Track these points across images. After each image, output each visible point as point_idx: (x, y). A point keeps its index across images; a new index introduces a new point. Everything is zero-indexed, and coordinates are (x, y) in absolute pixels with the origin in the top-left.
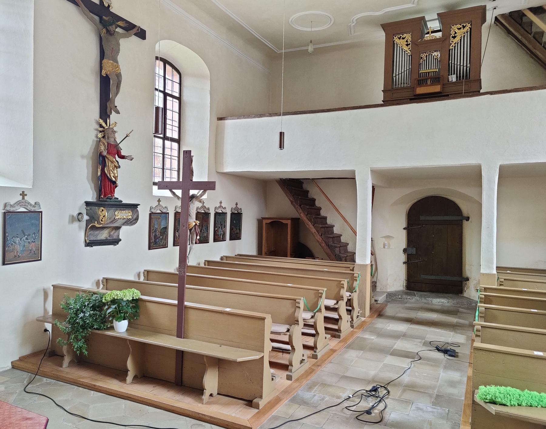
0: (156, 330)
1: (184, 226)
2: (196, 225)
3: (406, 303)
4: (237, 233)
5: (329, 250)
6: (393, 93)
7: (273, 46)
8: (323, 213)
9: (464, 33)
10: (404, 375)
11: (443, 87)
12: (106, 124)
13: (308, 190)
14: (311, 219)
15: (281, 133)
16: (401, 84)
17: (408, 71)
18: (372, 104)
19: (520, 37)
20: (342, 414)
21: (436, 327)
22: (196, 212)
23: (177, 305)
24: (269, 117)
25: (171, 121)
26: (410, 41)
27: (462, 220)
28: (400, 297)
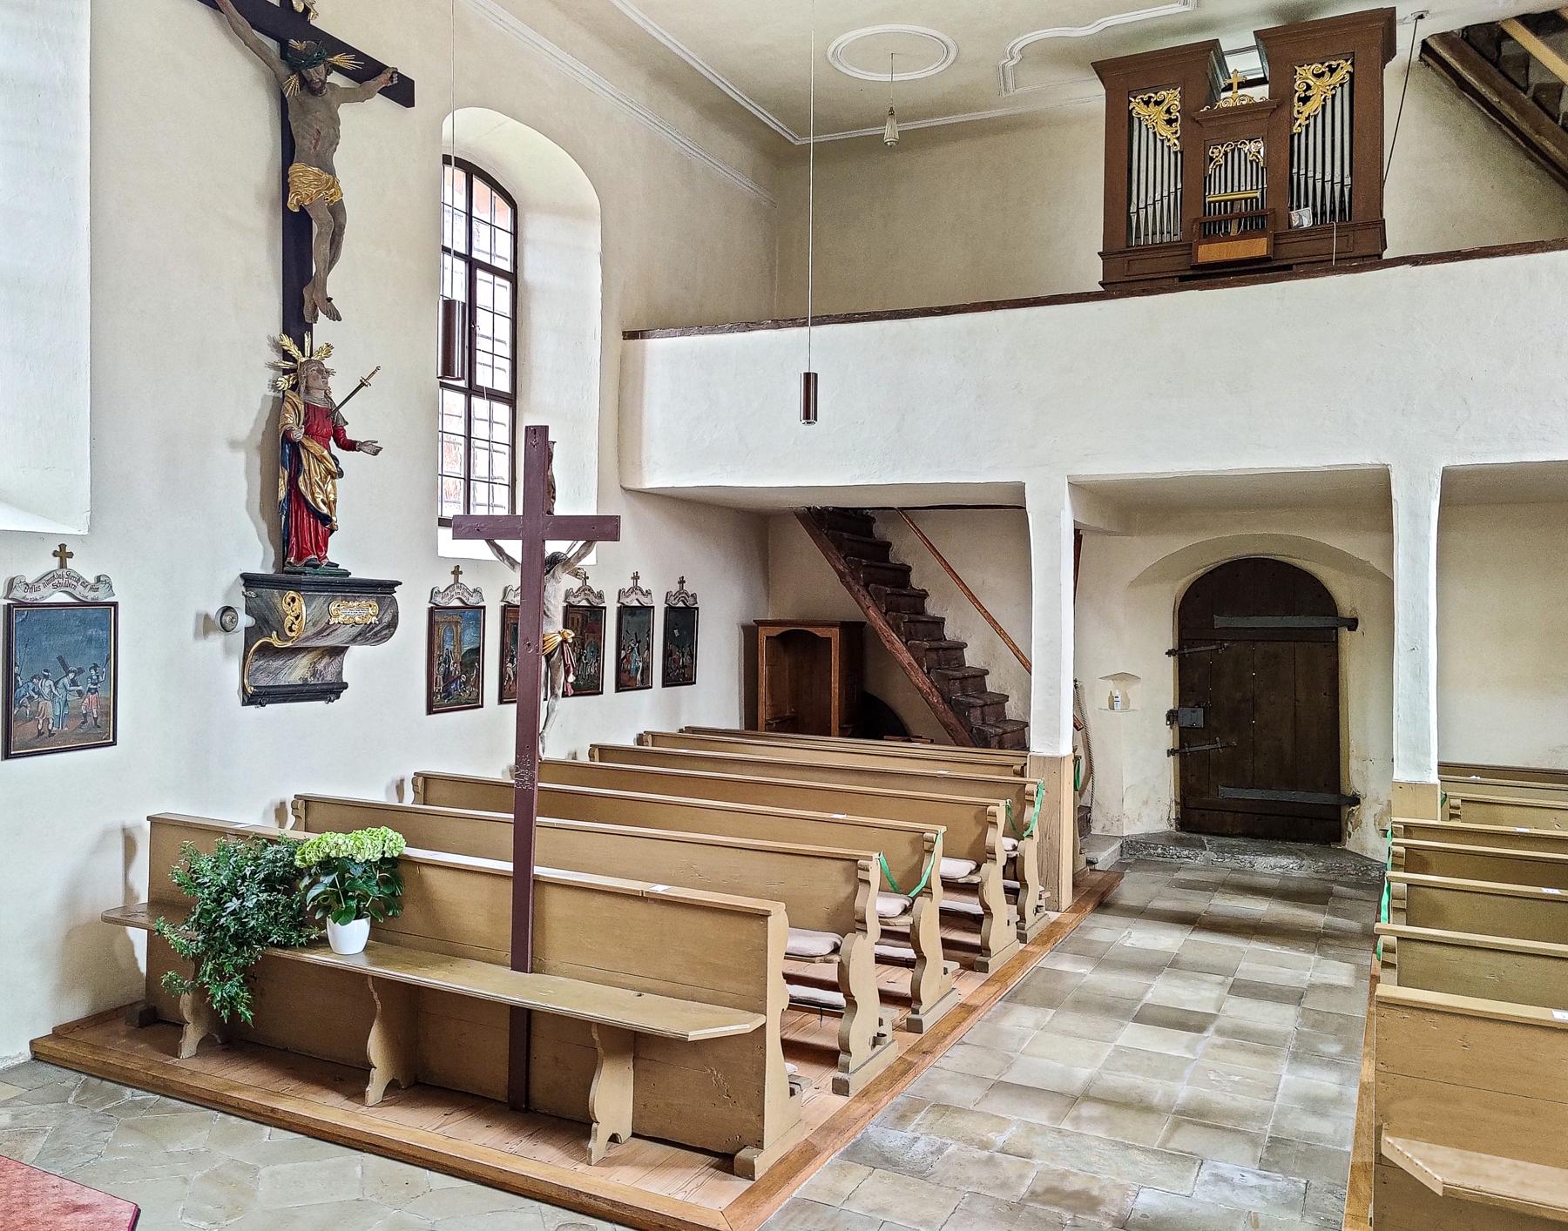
0: (451, 950)
1: (529, 645)
2: (565, 641)
3: (1179, 869)
5: (951, 714)
8: (932, 608)
9: (1334, 88)
12: (302, 349)
14: (898, 627)
15: (807, 376)
16: (1154, 233)
17: (1172, 197)
21: (1266, 941)
22: (565, 604)
26: (1179, 111)
27: (1337, 629)
28: (1159, 851)
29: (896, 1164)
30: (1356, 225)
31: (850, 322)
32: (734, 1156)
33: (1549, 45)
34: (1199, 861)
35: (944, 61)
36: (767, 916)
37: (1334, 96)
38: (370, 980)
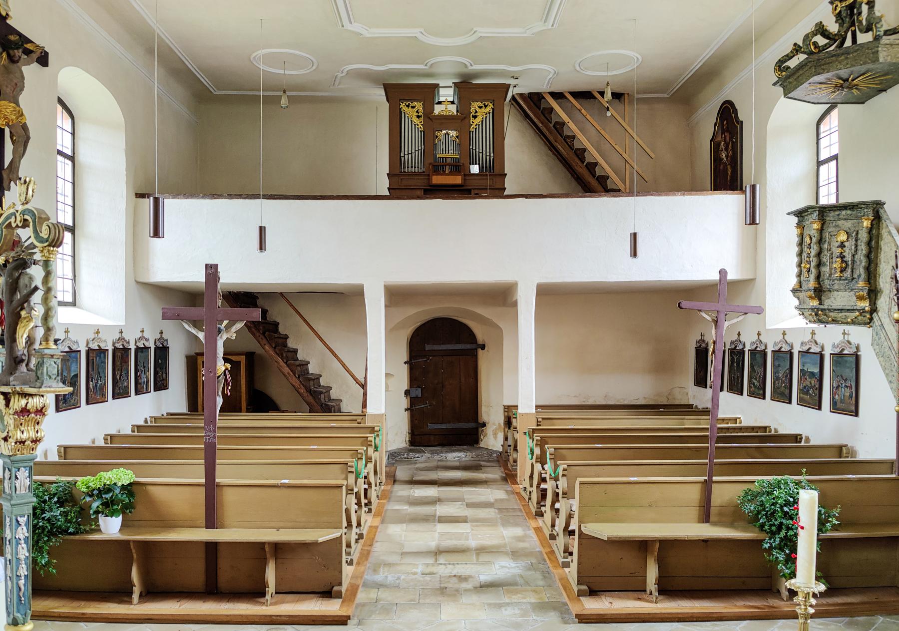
0: (169, 524)
1: (210, 372)
2: (227, 369)
5: (311, 397)
6: (401, 179)
7: (209, 83)
8: (291, 344)
9: (486, 114)
11: (464, 179)
14: (282, 354)
15: (261, 228)
16: (412, 167)
17: (420, 151)
18: (384, 195)
19: (540, 125)
21: (468, 487)
22: (87, 349)
23: (204, 484)
24: (229, 199)
25: (63, 196)
27: (477, 349)
28: (406, 456)
29: (386, 586)
30: (496, 175)
31: (273, 199)
32: (331, 592)
34: (423, 459)
35: (311, 68)
36: (342, 487)
37: (486, 117)
38: (132, 544)
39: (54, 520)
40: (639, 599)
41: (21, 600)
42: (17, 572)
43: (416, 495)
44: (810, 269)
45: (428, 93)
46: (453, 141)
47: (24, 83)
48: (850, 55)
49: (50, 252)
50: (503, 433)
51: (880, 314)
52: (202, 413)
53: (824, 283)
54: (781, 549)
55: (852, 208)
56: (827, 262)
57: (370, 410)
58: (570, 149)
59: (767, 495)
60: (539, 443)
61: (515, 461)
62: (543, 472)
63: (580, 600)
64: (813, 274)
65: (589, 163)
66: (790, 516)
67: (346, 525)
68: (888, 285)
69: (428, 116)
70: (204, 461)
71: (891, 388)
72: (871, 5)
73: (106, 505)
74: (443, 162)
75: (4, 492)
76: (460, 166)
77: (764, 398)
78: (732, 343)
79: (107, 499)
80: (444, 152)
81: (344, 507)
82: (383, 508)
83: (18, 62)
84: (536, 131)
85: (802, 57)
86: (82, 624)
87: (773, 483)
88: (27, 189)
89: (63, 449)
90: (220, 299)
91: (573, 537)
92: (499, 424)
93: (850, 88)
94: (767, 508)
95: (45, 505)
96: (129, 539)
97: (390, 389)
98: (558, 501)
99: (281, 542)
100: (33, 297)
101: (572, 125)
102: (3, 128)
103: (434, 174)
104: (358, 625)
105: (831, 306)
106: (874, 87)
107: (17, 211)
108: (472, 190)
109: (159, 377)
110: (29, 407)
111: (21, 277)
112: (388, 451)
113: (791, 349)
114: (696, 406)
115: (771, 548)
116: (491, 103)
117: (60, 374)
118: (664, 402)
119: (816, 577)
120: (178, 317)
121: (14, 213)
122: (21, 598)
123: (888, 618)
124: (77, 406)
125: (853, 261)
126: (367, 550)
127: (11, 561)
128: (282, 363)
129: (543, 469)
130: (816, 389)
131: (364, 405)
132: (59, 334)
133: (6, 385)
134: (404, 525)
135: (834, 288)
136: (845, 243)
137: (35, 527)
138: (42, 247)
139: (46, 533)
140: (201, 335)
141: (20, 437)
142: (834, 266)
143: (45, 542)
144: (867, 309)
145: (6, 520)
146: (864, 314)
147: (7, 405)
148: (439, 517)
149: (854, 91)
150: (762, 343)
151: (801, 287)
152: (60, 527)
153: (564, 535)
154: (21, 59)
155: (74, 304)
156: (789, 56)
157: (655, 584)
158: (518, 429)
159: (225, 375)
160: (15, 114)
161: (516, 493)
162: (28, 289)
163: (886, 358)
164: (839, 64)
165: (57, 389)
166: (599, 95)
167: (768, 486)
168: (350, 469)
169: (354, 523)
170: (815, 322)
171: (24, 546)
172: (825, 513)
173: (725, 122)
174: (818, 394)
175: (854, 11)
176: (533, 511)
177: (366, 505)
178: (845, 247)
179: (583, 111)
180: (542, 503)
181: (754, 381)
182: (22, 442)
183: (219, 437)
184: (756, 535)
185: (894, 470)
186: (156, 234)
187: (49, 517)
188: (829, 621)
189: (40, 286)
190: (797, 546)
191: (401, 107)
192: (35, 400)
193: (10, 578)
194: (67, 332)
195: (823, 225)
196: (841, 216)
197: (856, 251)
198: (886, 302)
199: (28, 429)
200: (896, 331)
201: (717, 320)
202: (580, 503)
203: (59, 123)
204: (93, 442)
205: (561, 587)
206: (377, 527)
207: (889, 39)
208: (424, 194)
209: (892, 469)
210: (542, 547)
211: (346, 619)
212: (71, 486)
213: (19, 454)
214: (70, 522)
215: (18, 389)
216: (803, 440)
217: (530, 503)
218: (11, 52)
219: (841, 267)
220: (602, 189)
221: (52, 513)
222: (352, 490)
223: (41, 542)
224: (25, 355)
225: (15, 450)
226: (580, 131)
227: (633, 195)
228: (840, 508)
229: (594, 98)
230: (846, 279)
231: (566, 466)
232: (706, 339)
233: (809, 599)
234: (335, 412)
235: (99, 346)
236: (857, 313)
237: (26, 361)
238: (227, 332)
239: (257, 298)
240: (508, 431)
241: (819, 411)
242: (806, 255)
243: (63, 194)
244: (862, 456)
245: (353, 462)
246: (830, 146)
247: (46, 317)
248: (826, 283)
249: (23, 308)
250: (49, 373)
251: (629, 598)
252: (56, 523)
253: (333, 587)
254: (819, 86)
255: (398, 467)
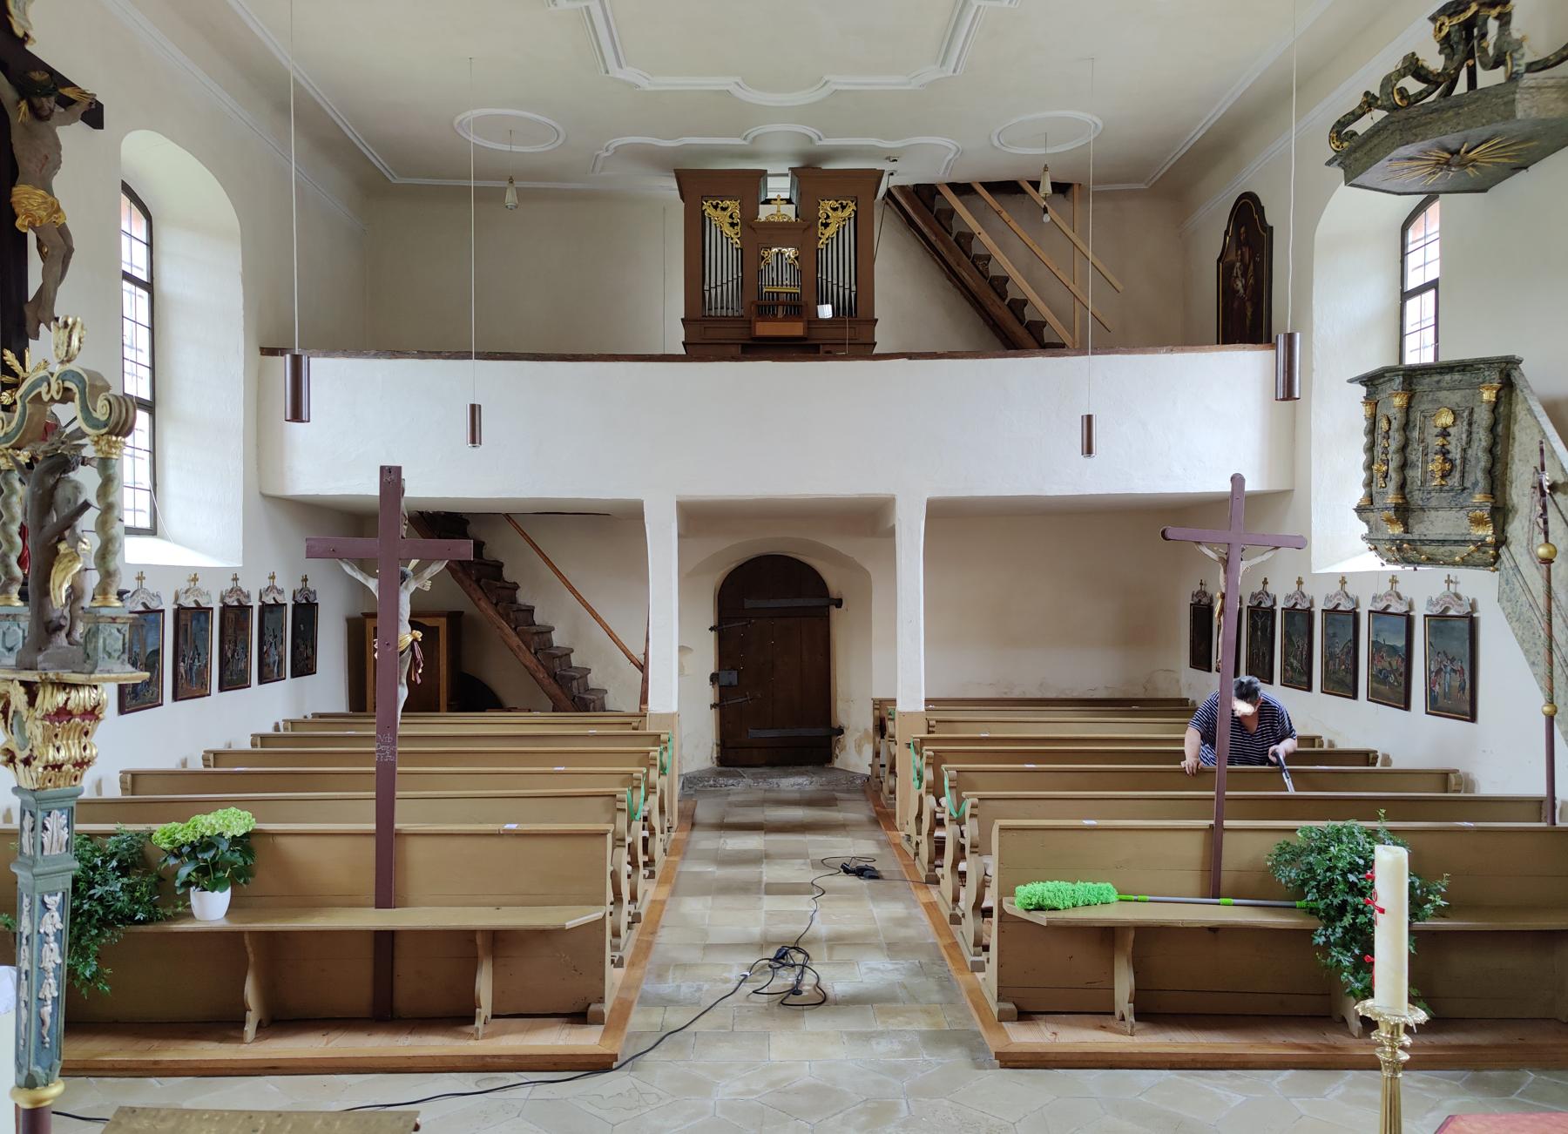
2: (415, 640)
3: (729, 794)
4: (308, 658)
8: (523, 597)
9: (844, 220)
10: (813, 923)
11: (808, 329)
12: (23, 364)
13: (483, 540)
14: (508, 615)
15: (473, 407)
16: (722, 308)
18: (677, 353)
19: (933, 238)
20: (747, 1004)
21: (815, 834)
22: (222, 605)
24: (419, 358)
27: (828, 607)
28: (712, 782)
30: (860, 321)
33: (960, 200)
34: (741, 787)
37: (844, 226)
38: (246, 937)
39: (110, 899)
40: (1103, 1028)
41: (43, 1043)
42: (38, 992)
43: (728, 848)
44: (1387, 473)
45: (749, 185)
46: (790, 264)
47: (60, 156)
48: (1463, 108)
49: (112, 444)
50: (872, 745)
51: (1512, 548)
52: (373, 714)
53: (1412, 496)
54: (1346, 946)
55: (1463, 370)
56: (1418, 461)
57: (654, 706)
58: (982, 278)
59: (1319, 854)
60: (931, 761)
61: (893, 792)
62: (938, 809)
63: (1003, 1028)
64: (1393, 482)
65: (1013, 301)
66: (1359, 890)
67: (613, 899)
68: (1526, 500)
69: (749, 223)
70: (375, 793)
71: (1535, 675)
72: (1503, 21)
73: (203, 871)
74: (773, 299)
75: (21, 853)
76: (801, 306)
77: (1309, 689)
78: (1253, 596)
79: (205, 861)
80: (775, 283)
81: (609, 869)
82: (674, 869)
83: (47, 118)
84: (925, 248)
85: (1378, 115)
86: (153, 1080)
87: (1329, 833)
88: (70, 337)
89: (129, 776)
90: (405, 524)
91: (989, 919)
92: (866, 730)
93: (1463, 165)
94: (1319, 875)
95: (94, 874)
96: (242, 929)
97: (686, 673)
98: (964, 858)
99: (501, 928)
100: (80, 519)
101: (985, 238)
102: (24, 231)
103: (759, 319)
104: (630, 1071)
105: (1425, 535)
106: (1504, 163)
107: (52, 374)
108: (821, 347)
109: (301, 654)
110: (71, 705)
111: (60, 485)
112: (683, 775)
113: (1355, 606)
114: (1194, 702)
115: (1328, 943)
116: (852, 202)
117: (127, 650)
118: (1139, 694)
119: (1409, 997)
120: (334, 554)
121: (47, 377)
122: (44, 1038)
123: (1544, 1075)
124: (156, 703)
125: (1464, 460)
126: (647, 941)
127: (29, 973)
128: (508, 630)
129: (939, 804)
130: (1401, 675)
131: (644, 699)
132: (126, 582)
133: (30, 669)
134: (709, 899)
135: (1430, 505)
136: (1450, 430)
137: (75, 912)
138: (97, 436)
139: (94, 921)
140: (373, 584)
141: (54, 757)
142: (1431, 467)
143: (92, 938)
144: (1489, 539)
145: (22, 902)
146: (1484, 549)
147: (32, 702)
148: (767, 885)
149: (1470, 171)
150: (1304, 597)
151: (1372, 504)
152: (120, 911)
153: (974, 915)
154: (54, 113)
155: (152, 531)
156: (1356, 114)
157: (1129, 1003)
158: (897, 738)
159: (412, 649)
160: (45, 209)
161: (895, 845)
162: (72, 507)
163: (1525, 624)
164: (1443, 126)
165: (123, 676)
166: (1030, 186)
167: (1320, 838)
168: (619, 805)
169: (626, 896)
170: (1396, 562)
171: (54, 946)
172: (1421, 887)
173: (1243, 229)
174: (1403, 683)
175: (1473, 32)
176: (923, 875)
177: (645, 864)
178: (1449, 435)
179: (1004, 214)
180: (937, 862)
181: (1292, 660)
182: (57, 766)
183: (400, 753)
184: (1300, 921)
185: (1543, 816)
186: (297, 415)
187: (102, 895)
188: (1436, 1076)
189: (93, 500)
190: (1373, 942)
191: (704, 208)
192: (81, 694)
193: (26, 1003)
194: (140, 578)
195: (1410, 400)
196: (1443, 384)
197: (1469, 442)
198: (1523, 528)
199: (68, 744)
200: (1543, 577)
201: (1228, 558)
202: (1001, 862)
203: (125, 226)
204: (184, 764)
205: (970, 1005)
206: (663, 903)
207: (1535, 79)
208: (742, 353)
209: (1541, 813)
210: (937, 936)
211: (609, 1061)
212: (142, 840)
213: (51, 787)
214: (138, 901)
215: (51, 675)
216: (1379, 760)
217: (917, 861)
218: (36, 101)
219: (1443, 470)
220: (1036, 344)
221: (107, 888)
222: (624, 840)
223: (85, 938)
224: (65, 617)
225: (44, 780)
226: (999, 248)
227: (1086, 354)
228: (1448, 878)
229: (1022, 191)
230: (1452, 490)
231: (976, 800)
232: (1209, 590)
233: (1398, 1035)
234: (595, 711)
235: (196, 602)
236: (1472, 547)
237: (67, 628)
238: (416, 579)
239: (467, 522)
240: (880, 742)
241: (1355, 701)
242: (1380, 450)
243: (135, 346)
244: (1485, 789)
245: (624, 793)
246: (1424, 264)
247: (105, 553)
248: (1416, 497)
249: (61, 539)
250: (107, 649)
251: (1085, 1026)
252: (113, 905)
253: (589, 1005)
254: (1407, 164)
255: (699, 803)
